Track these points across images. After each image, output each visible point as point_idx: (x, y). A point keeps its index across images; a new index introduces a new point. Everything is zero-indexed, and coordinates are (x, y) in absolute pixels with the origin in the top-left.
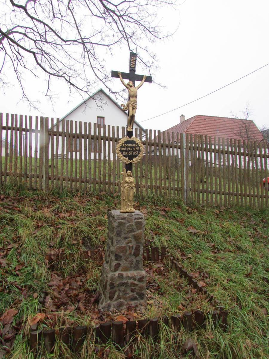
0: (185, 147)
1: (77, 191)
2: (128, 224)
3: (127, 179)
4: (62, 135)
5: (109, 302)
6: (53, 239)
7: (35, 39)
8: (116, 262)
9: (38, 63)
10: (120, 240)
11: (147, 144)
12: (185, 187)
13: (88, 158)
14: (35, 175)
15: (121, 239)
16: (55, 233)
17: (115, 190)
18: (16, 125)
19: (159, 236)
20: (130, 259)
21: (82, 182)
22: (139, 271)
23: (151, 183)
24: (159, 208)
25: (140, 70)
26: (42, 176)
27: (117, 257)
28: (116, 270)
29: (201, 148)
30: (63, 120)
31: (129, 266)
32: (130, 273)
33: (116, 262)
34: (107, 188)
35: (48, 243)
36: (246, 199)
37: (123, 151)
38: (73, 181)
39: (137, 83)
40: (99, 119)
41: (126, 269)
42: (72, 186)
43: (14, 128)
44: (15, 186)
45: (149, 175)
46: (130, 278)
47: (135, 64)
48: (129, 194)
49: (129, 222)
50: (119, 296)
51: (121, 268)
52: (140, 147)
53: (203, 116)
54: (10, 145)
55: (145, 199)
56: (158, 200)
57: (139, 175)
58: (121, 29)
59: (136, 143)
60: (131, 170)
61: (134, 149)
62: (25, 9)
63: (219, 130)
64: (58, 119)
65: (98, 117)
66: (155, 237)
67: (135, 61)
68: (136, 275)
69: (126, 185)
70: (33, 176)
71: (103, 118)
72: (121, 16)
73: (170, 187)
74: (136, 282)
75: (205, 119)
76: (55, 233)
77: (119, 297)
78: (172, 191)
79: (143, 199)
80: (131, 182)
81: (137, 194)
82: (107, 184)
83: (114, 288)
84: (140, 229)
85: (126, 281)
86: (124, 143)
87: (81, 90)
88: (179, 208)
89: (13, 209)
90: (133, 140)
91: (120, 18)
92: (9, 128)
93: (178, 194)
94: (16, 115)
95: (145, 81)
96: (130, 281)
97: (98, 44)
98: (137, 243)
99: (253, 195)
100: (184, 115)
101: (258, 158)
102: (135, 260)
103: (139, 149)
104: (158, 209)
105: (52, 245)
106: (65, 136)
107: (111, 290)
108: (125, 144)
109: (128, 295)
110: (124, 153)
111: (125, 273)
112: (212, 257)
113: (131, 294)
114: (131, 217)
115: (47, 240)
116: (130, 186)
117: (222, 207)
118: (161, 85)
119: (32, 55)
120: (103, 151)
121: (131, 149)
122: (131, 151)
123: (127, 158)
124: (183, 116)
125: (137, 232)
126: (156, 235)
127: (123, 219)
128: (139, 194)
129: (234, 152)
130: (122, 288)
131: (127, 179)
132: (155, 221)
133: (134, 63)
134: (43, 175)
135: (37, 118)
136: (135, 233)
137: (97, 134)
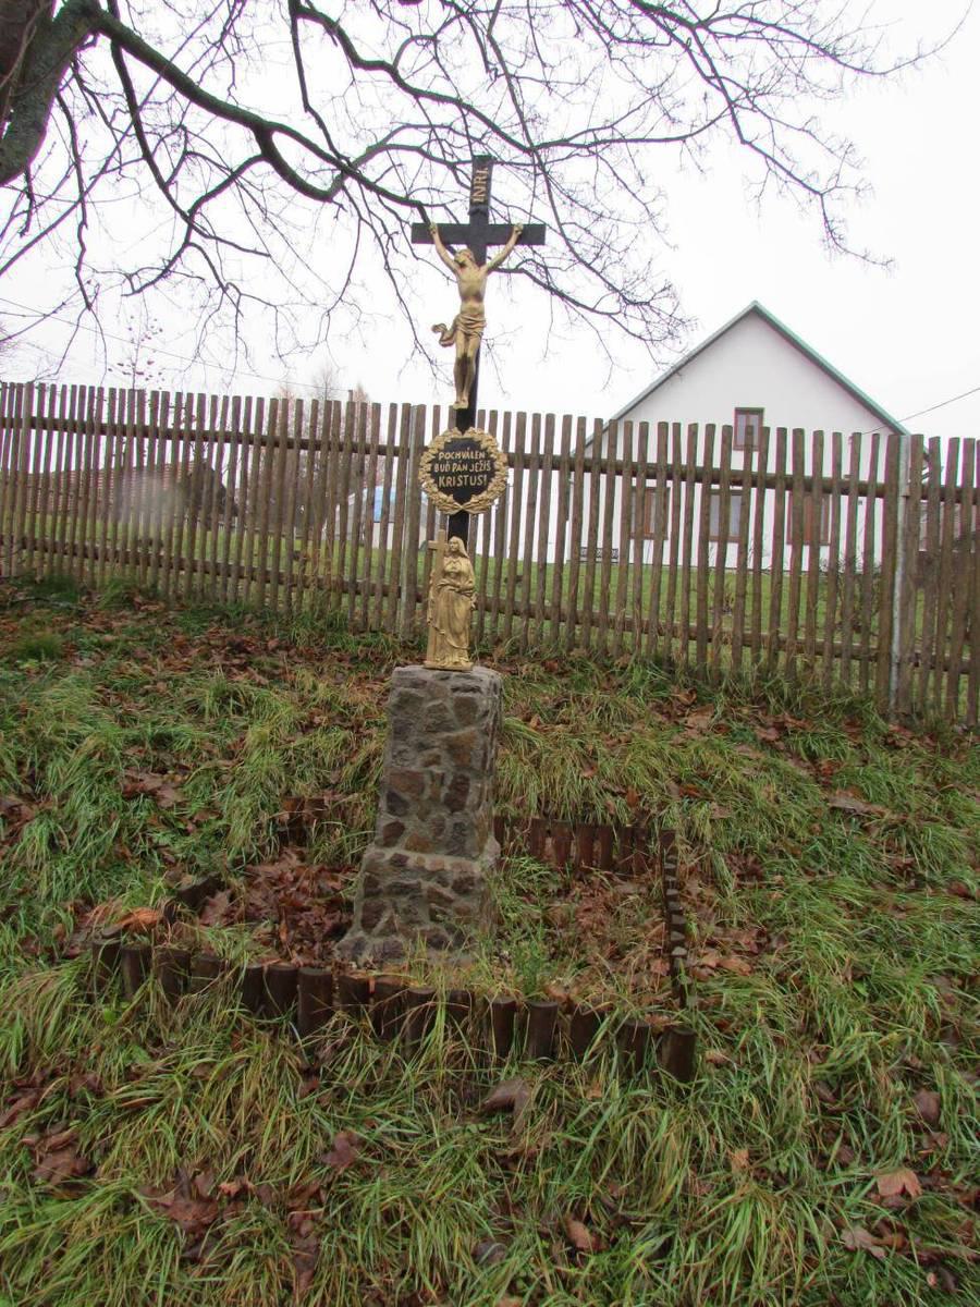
0: (904, 490)
1: (498, 642)
2: (431, 704)
5: (361, 934)
8: (392, 819)
10: (405, 751)
12: (895, 648)
14: (378, 587)
15: (409, 749)
17: (621, 647)
20: (434, 816)
21: (516, 613)
22: (462, 860)
26: (396, 589)
27: (396, 805)
30: (614, 423)
31: (431, 836)
32: (429, 861)
33: (392, 819)
34: (594, 637)
37: (440, 474)
40: (743, 418)
41: (421, 846)
46: (431, 875)
49: (434, 698)
50: (390, 923)
51: (405, 839)
52: (493, 461)
58: (709, 73)
59: (483, 446)
61: (475, 468)
62: (392, 70)
64: (598, 422)
65: (739, 411)
68: (448, 867)
69: (446, 581)
72: (705, 24)
74: (447, 892)
77: (390, 929)
78: (837, 662)
80: (459, 574)
83: (377, 894)
84: (469, 723)
85: (413, 882)
86: (442, 447)
87: (593, 310)
88: (852, 724)
90: (471, 439)
91: (701, 33)
93: (865, 676)
96: (426, 885)
98: (458, 767)
102: (449, 822)
103: (492, 466)
105: (333, 782)
107: (368, 900)
110: (441, 479)
111: (413, 858)
112: (858, 899)
113: (429, 926)
114: (441, 683)
116: (454, 585)
120: (394, 483)
121: (465, 468)
122: (463, 473)
123: (451, 498)
125: (460, 732)
127: (415, 685)
130: (403, 902)
131: (449, 564)
133: (483, 189)
134: (400, 589)
135: (393, 407)
136: (453, 735)
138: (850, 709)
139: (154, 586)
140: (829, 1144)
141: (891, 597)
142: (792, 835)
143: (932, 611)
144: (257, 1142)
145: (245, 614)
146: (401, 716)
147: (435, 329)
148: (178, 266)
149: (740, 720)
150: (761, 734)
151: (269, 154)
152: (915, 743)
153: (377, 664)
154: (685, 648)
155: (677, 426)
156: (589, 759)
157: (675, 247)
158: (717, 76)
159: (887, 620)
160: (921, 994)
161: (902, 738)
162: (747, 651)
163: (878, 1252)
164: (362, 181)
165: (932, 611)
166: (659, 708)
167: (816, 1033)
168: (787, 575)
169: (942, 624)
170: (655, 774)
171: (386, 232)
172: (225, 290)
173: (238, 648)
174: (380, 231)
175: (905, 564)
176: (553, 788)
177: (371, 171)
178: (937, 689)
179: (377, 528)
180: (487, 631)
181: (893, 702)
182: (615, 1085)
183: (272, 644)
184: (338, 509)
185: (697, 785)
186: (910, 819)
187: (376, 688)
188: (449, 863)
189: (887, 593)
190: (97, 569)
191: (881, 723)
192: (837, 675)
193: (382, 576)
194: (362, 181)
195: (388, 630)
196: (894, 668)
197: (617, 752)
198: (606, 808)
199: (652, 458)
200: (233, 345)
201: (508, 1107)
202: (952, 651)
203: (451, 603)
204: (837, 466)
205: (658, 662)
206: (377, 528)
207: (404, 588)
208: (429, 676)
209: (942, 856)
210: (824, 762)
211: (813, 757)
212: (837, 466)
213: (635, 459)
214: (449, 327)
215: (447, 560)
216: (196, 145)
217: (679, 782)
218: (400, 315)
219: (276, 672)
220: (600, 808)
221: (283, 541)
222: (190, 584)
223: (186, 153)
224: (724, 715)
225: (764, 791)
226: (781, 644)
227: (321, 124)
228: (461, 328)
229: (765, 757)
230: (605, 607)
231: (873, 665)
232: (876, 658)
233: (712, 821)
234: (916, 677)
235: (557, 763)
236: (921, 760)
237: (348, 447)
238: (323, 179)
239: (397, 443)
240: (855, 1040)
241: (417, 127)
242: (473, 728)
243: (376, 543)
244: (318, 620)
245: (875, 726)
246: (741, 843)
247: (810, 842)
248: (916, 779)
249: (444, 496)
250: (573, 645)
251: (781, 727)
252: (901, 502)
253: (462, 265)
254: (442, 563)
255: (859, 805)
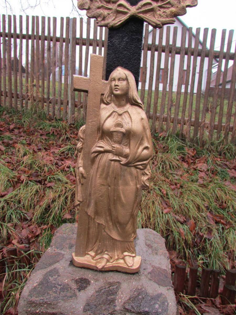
4: (93, 44)
13: (154, 88)
14: (59, 101)
16: (39, 195)
17: (162, 130)
18: (38, 32)
19: (223, 228)
23: (220, 121)
24: (227, 163)
43: (35, 36)
45: (218, 108)
48: (116, 190)
55: (207, 146)
56: (227, 149)
66: (214, 227)
69: (104, 145)
76: (39, 195)
79: (203, 145)
81: (194, 137)
92: (30, 37)
94: (37, 17)
104: (226, 165)
106: (103, 46)
126: (217, 223)
128: (198, 136)
132: (219, 193)
134: (68, 101)
153: (58, 137)
187: (56, 151)
193: (60, 96)
195: (64, 119)
200: (5, 5)
207: (70, 101)
219: (11, 142)
237: (43, 38)
239: (64, 36)
244: (34, 114)
254: (98, 115)
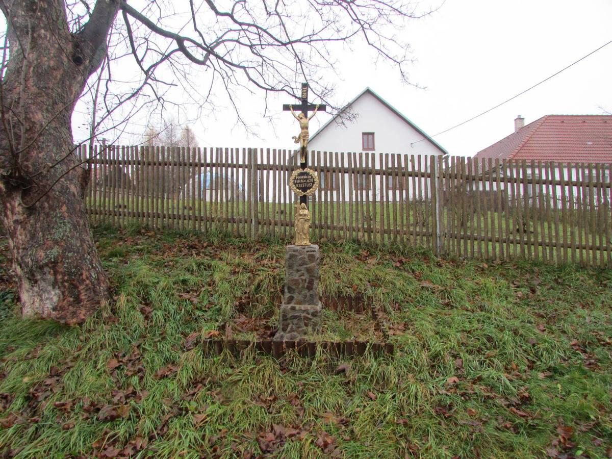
0: (437, 175)
3: (301, 212)
5: (282, 333)
6: (249, 286)
7: (250, 44)
9: (250, 79)
11: (382, 173)
14: (243, 219)
17: (339, 236)
18: (221, 161)
20: (303, 293)
22: (313, 306)
25: (312, 99)
28: (289, 303)
29: (461, 175)
32: (303, 307)
35: (243, 288)
36: (536, 249)
38: (287, 225)
39: (310, 113)
41: (300, 303)
42: (285, 231)
44: (220, 233)
47: (307, 95)
49: (301, 255)
51: (294, 301)
53: (558, 116)
54: (595, 194)
57: (411, 222)
58: (355, 18)
60: (306, 203)
61: (308, 181)
63: (592, 140)
65: (364, 134)
67: (307, 91)
68: (309, 308)
70: (240, 221)
71: (373, 134)
73: (414, 231)
74: (310, 316)
75: (563, 122)
77: (292, 330)
78: (418, 237)
80: (305, 215)
82: (328, 228)
83: (286, 320)
84: (313, 262)
88: (425, 259)
89: (213, 257)
91: (351, 4)
92: (214, 165)
93: (428, 241)
94: (221, 149)
95: (318, 110)
96: (303, 315)
97: (329, 40)
98: (310, 276)
99: (549, 243)
100: (522, 117)
101: (557, 186)
102: (308, 295)
108: (298, 176)
109: (301, 329)
111: (297, 307)
115: (242, 285)
117: (495, 260)
118: (419, 86)
119: (242, 70)
124: (520, 119)
127: (294, 251)
129: (516, 179)
130: (295, 321)
131: (301, 212)
135: (244, 149)
136: (308, 266)
137: (328, 165)
138: (424, 254)
139: (147, 225)
140: (433, 372)
141: (435, 213)
142: (410, 296)
143: (450, 217)
144: (274, 387)
145: (189, 234)
146: (291, 261)
147: (293, 138)
148: (141, 92)
149: (386, 260)
150: (394, 264)
151: (182, 49)
152: (447, 264)
154: (364, 235)
155: (355, 154)
156: (338, 276)
157: (344, 80)
158: (358, 19)
159: (434, 221)
160: (455, 337)
161: (442, 263)
162: (386, 235)
163: (449, 394)
164: (217, 57)
165: (450, 217)
166: (357, 258)
167: (425, 346)
168: (398, 203)
169: (453, 221)
170: (361, 280)
171: (227, 75)
172: (159, 100)
173: (192, 247)
174: (225, 75)
175: (439, 201)
176: (327, 287)
177: (220, 50)
178: (453, 245)
179: (208, 192)
180: (287, 233)
181: (438, 251)
182: (373, 360)
183: (205, 245)
184: (186, 185)
185: (376, 282)
186: (448, 288)
188: (309, 307)
189: (434, 208)
190: (121, 220)
191: (435, 258)
192: (418, 242)
194: (217, 57)
196: (438, 239)
197: (347, 273)
198: (346, 292)
199: (346, 166)
201: (343, 371)
202: (457, 231)
203: (303, 224)
204: (413, 167)
205: (354, 241)
206: (208, 192)
208: (298, 248)
209: (459, 299)
210: (417, 273)
211: (413, 271)
212: (413, 167)
213: (340, 166)
214: (297, 137)
215: (301, 211)
216: (151, 46)
217: (369, 282)
218: (231, 107)
220: (344, 292)
221: (202, 202)
222: (163, 224)
223: (147, 49)
224: (381, 258)
225: (399, 283)
226: (398, 232)
227: (201, 35)
228: (302, 138)
229: (397, 272)
230: (332, 222)
231: (431, 239)
232: (432, 235)
233: (383, 294)
234: (446, 242)
235: (327, 278)
236: (449, 270)
238: (199, 54)
239: (247, 163)
240: (437, 346)
241: (235, 31)
242: (314, 263)
243: (208, 199)
245: (433, 259)
246: (393, 300)
247: (416, 298)
248: (448, 276)
249: (298, 190)
250: (321, 237)
251: (401, 262)
252: (436, 179)
253: (301, 118)
255: (431, 285)
